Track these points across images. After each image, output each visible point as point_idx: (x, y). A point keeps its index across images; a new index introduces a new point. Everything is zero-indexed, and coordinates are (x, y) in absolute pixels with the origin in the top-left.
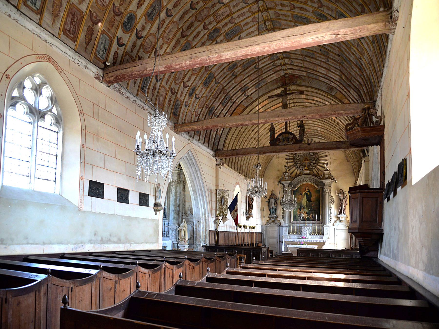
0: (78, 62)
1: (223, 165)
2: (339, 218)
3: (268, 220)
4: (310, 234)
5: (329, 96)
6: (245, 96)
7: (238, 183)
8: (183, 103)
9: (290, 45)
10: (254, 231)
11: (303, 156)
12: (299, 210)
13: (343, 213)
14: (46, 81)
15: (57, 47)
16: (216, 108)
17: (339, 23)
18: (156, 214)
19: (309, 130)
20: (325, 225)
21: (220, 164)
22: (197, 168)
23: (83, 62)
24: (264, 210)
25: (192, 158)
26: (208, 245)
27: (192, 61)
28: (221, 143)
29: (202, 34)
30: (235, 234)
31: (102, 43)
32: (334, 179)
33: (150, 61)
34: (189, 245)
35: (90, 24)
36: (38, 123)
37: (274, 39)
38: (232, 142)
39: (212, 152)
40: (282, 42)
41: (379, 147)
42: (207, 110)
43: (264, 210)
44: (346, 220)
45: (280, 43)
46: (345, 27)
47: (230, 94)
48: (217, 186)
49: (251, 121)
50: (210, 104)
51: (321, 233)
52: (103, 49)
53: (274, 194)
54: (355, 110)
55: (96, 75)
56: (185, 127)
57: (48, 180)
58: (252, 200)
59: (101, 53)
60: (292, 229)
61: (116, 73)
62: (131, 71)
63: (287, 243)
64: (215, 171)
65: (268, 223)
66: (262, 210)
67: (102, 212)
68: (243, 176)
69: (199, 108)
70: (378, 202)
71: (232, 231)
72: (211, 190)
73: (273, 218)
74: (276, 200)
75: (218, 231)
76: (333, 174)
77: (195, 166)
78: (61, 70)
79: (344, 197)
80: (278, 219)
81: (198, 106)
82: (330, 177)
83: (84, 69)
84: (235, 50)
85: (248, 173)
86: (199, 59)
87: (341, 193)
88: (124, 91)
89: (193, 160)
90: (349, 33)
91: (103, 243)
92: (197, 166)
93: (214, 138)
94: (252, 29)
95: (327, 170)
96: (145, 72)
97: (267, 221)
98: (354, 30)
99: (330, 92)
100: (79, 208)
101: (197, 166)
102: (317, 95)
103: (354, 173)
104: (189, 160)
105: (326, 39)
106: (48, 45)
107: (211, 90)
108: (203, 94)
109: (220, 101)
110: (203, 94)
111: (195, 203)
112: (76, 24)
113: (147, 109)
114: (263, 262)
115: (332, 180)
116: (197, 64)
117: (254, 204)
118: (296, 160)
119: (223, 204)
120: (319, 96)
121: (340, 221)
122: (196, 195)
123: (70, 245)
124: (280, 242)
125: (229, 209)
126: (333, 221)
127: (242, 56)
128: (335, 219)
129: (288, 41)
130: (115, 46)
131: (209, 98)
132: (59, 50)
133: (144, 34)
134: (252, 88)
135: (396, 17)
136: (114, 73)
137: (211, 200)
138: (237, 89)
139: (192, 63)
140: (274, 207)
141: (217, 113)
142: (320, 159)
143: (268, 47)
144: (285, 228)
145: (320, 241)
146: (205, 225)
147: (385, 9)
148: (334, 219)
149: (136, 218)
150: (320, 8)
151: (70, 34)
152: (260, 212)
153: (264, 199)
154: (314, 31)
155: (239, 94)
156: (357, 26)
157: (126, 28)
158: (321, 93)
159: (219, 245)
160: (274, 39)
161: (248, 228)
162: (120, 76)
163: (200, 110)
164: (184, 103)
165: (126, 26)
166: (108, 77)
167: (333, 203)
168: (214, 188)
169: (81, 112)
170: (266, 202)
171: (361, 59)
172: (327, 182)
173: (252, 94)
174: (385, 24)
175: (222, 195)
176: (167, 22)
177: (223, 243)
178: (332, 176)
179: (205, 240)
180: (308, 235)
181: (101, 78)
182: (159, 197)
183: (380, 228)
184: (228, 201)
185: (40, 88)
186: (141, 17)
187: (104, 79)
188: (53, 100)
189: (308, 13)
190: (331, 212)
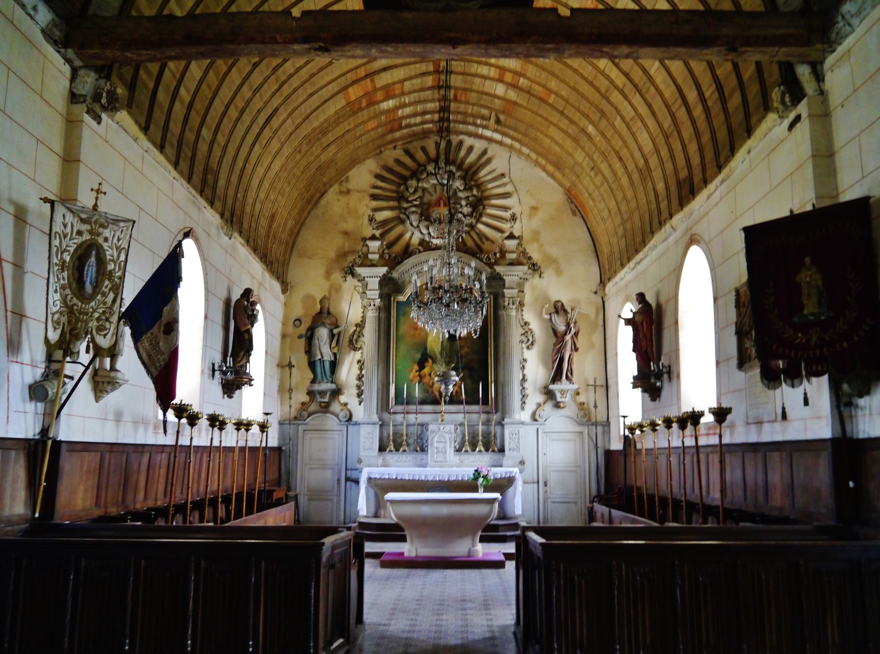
2: (549, 395)
3: (303, 404)
4: (458, 450)
10: (254, 438)
11: (431, 190)
12: (416, 367)
13: (567, 377)
20: (510, 417)
21: (97, 97)
24: (290, 366)
30: (164, 456)
32: (535, 267)
43: (290, 366)
53: (329, 313)
58: (253, 319)
60: (394, 434)
63: (381, 487)
65: (305, 414)
66: (285, 366)
68: (218, 217)
71: (140, 441)
74: (335, 331)
75: (57, 444)
80: (343, 399)
82: (524, 259)
85: (237, 213)
87: (557, 312)
95: (511, 236)
97: (299, 406)
117: (259, 332)
118: (408, 201)
119: (88, 288)
121: (557, 406)
124: (348, 479)
126: (530, 406)
128: (541, 398)
140: (328, 356)
142: (486, 202)
144: (369, 428)
148: (535, 398)
152: (276, 372)
153: (291, 329)
159: (57, 520)
161: (230, 428)
167: (532, 344)
170: (300, 337)
172: (511, 275)
175: (86, 237)
177: (89, 502)
180: (451, 451)
184: (122, 278)
190: (524, 376)
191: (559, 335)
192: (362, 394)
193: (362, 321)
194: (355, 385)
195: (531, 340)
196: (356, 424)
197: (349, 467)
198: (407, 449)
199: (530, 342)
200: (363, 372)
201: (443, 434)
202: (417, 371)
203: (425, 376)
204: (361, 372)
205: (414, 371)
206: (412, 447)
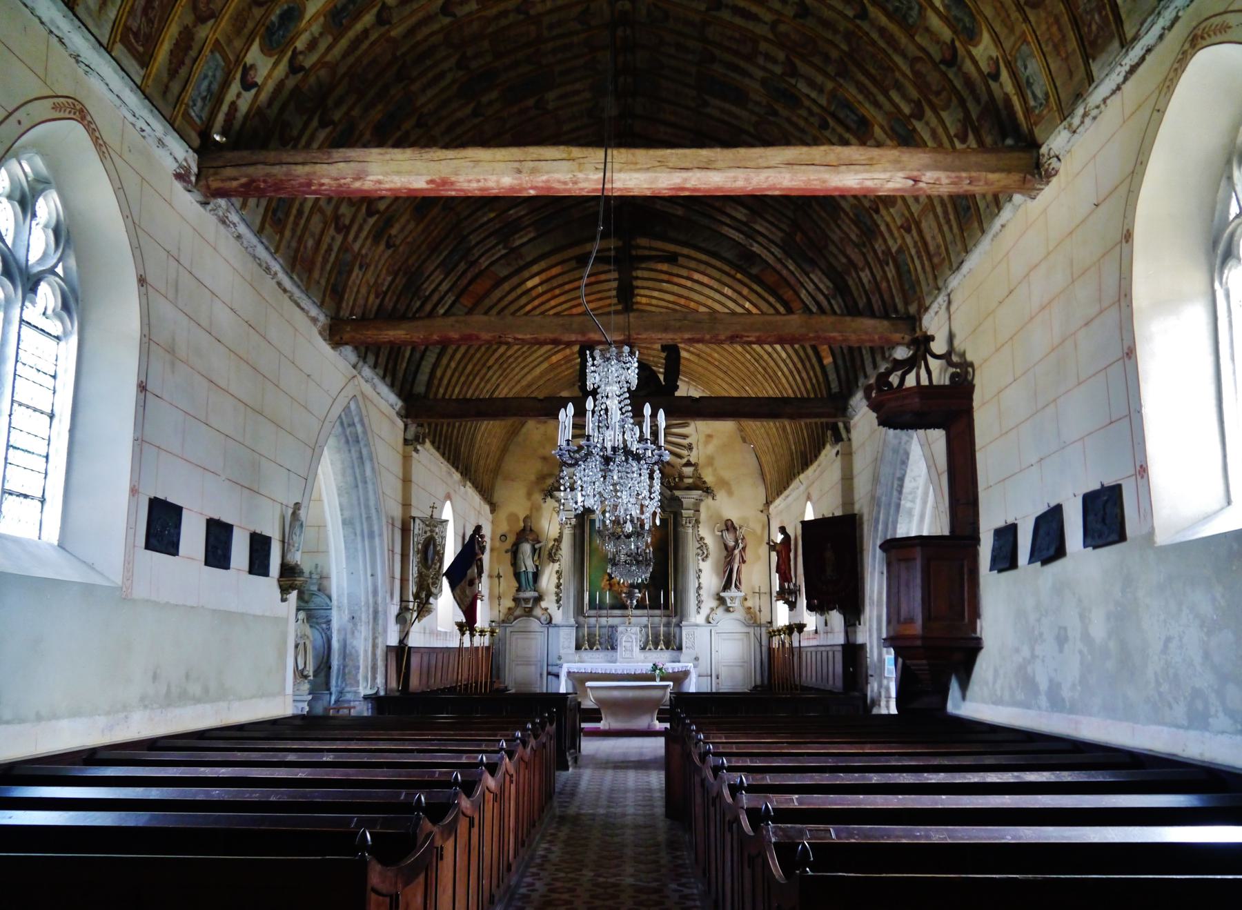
0: (145, 127)
1: (423, 443)
2: (722, 601)
3: (510, 609)
4: (643, 649)
5: (739, 276)
6: (504, 248)
7: (448, 497)
8: (355, 258)
9: (802, 185)
14: (52, 180)
15: (103, 79)
17: (923, 155)
18: (283, 600)
22: (365, 452)
23: (158, 127)
24: (499, 576)
26: (382, 693)
27: (520, 178)
28: (423, 377)
29: (449, 78)
31: (206, 76)
33: (380, 157)
34: (310, 697)
35: (189, 19)
36: (22, 310)
37: (762, 163)
39: (399, 404)
40: (783, 175)
41: (938, 437)
44: (742, 605)
45: (777, 175)
46: (936, 167)
48: (406, 505)
51: (672, 643)
52: (205, 94)
53: (531, 530)
55: (181, 166)
57: (26, 496)
59: (199, 103)
60: (589, 634)
61: (251, 170)
62: (308, 174)
64: (399, 458)
65: (512, 618)
67: (172, 602)
69: (388, 273)
72: (393, 519)
73: (526, 600)
74: (537, 546)
77: (362, 444)
78: (105, 151)
79: (736, 541)
80: (544, 604)
81: (387, 269)
83: (155, 147)
84: (656, 172)
86: (544, 178)
87: (728, 530)
88: (234, 217)
90: (945, 181)
91: (169, 705)
92: (367, 445)
94: (578, 86)
95: (688, 464)
96: (357, 185)
98: (957, 177)
100: (124, 589)
101: (366, 445)
102: (702, 267)
104: (346, 425)
105: (891, 185)
106: (80, 70)
110: (406, 237)
112: (155, 16)
113: (276, 274)
114: (720, 738)
116: (532, 188)
119: (430, 562)
120: (710, 271)
121: (728, 610)
123: (97, 717)
124: (549, 674)
126: (705, 610)
127: (668, 189)
128: (714, 604)
129: (799, 175)
130: (235, 87)
132: (105, 87)
133: (309, 62)
134: (530, 229)
135: (1053, 169)
136: (244, 169)
137: (393, 551)
139: (520, 184)
143: (746, 180)
145: (673, 668)
147: (1020, 144)
148: (709, 603)
149: (242, 614)
150: (787, 78)
151: (137, 42)
154: (864, 162)
155: (493, 241)
156: (964, 170)
157: (271, 41)
160: (762, 163)
162: (265, 181)
163: (389, 279)
164: (359, 258)
165: (273, 34)
166: (218, 177)
167: (707, 557)
168: (397, 512)
169: (142, 281)
170: (507, 552)
171: (877, 211)
173: (523, 245)
174: (1025, 177)
175: (429, 534)
176: (374, 36)
179: (374, 678)
180: (636, 649)
181: (193, 179)
183: (973, 635)
185: (33, 196)
186: (314, 18)
187: (202, 183)
188: (61, 234)
189: (747, 81)
190: (699, 584)
191: (729, 549)
196: (556, 626)
200: (561, 581)
206: (604, 647)
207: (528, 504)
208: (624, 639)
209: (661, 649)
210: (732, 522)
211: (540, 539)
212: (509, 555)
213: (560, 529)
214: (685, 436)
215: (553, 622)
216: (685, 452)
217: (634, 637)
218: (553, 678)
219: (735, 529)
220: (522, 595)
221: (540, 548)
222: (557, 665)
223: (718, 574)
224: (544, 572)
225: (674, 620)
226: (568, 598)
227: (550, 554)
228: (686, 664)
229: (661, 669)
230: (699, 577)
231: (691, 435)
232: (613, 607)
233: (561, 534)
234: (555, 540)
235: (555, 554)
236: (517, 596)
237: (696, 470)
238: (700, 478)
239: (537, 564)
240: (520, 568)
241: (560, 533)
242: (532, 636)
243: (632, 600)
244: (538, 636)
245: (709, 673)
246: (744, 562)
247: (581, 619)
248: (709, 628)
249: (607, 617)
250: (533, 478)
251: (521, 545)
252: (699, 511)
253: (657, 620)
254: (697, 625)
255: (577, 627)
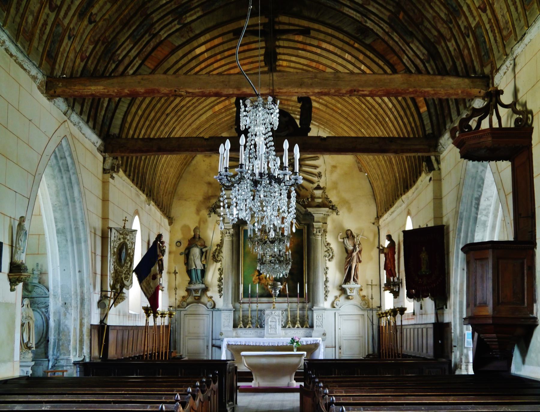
1: (118, 171)
2: (343, 291)
3: (183, 297)
4: (284, 327)
5: (356, 45)
6: (178, 24)
7: (137, 213)
8: (65, 31)
16: (120, 44)
18: (12, 290)
19: (286, 102)
22: (73, 178)
24: (175, 273)
25: (67, 154)
26: (87, 360)
28: (117, 121)
32: (333, 208)
34: (33, 363)
38: (137, 119)
42: (103, 48)
44: (359, 295)
47: (153, 19)
48: (105, 218)
49: (238, 88)
50: (112, 36)
53: (199, 238)
54: (452, 88)
56: (75, 86)
64: (100, 183)
65: (185, 304)
69: (91, 42)
70: (525, 266)
72: (95, 229)
73: (196, 291)
74: (204, 250)
75: (108, 326)
76: (334, 198)
77: (71, 172)
80: (209, 294)
82: (327, 204)
87: (348, 237)
89: (69, 159)
92: (75, 173)
93: (104, 109)
95: (318, 188)
99: (360, 38)
101: (74, 173)
102: (329, 38)
103: (374, 195)
104: (59, 158)
107: (120, 7)
108: (104, 15)
109: (131, 31)
110: (104, 15)
111: (61, 258)
114: (342, 392)
115: (330, 209)
120: (334, 41)
121: (348, 298)
122: (64, 242)
124: (213, 346)
125: (137, 274)
126: (331, 298)
128: (337, 293)
131: (114, 23)
134: (198, 9)
137: (95, 253)
138: (168, 8)
140: (199, 266)
141: (119, 55)
145: (307, 342)
146: (81, 313)
148: (334, 293)
155: (170, 18)
158: (341, 36)
167: (332, 258)
170: (181, 254)
172: (318, 213)
175: (122, 240)
178: (330, 202)
180: (279, 327)
182: (22, 248)
183: (531, 315)
190: (327, 278)
191: (349, 252)
192: (222, 291)
193: (221, 243)
194: (217, 285)
195: (331, 255)
196: (219, 310)
197: (214, 338)
198: (251, 326)
199: (330, 257)
200: (222, 276)
201: (275, 316)
202: (257, 276)
203: (263, 279)
204: (221, 276)
205: (255, 275)
207: (197, 218)
208: (270, 320)
209: (298, 327)
210: (351, 232)
211: (206, 244)
212: (182, 258)
213: (222, 237)
214: (316, 167)
215: (217, 307)
216: (315, 179)
217: (277, 318)
218: (217, 349)
219: (353, 237)
220: (193, 287)
221: (206, 251)
222: (219, 339)
223: (340, 271)
224: (209, 270)
225: (308, 306)
226: (228, 290)
227: (214, 256)
228: (317, 339)
229: (297, 342)
230: (326, 273)
231: (321, 166)
232: (261, 296)
233: (222, 240)
234: (218, 245)
235: (218, 256)
236: (189, 288)
237: (324, 192)
238: (327, 198)
239: (204, 263)
240: (191, 266)
241: (221, 240)
242: (201, 317)
243: (275, 291)
244: (205, 317)
245: (334, 345)
246: (360, 261)
247: (237, 305)
248: (334, 311)
249: (257, 303)
250: (200, 198)
251: (192, 249)
252: (326, 223)
253: (294, 305)
254: (325, 309)
255: (234, 311)
